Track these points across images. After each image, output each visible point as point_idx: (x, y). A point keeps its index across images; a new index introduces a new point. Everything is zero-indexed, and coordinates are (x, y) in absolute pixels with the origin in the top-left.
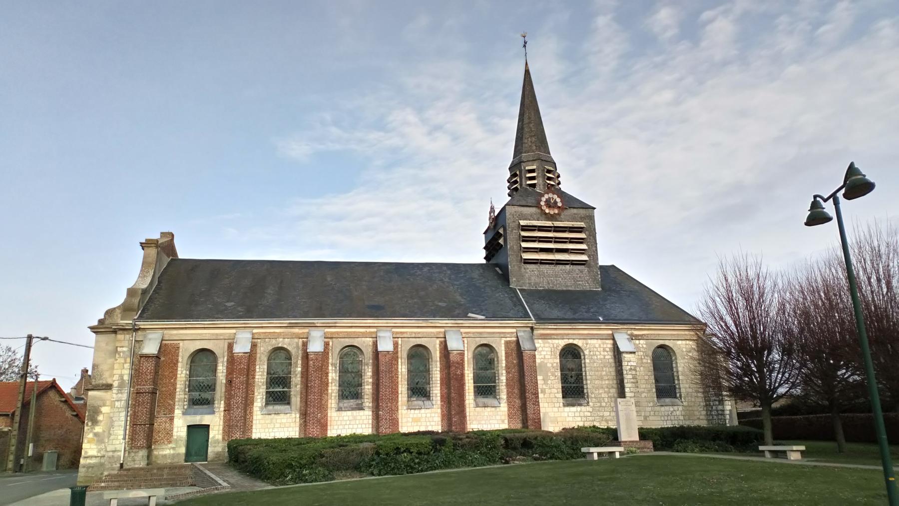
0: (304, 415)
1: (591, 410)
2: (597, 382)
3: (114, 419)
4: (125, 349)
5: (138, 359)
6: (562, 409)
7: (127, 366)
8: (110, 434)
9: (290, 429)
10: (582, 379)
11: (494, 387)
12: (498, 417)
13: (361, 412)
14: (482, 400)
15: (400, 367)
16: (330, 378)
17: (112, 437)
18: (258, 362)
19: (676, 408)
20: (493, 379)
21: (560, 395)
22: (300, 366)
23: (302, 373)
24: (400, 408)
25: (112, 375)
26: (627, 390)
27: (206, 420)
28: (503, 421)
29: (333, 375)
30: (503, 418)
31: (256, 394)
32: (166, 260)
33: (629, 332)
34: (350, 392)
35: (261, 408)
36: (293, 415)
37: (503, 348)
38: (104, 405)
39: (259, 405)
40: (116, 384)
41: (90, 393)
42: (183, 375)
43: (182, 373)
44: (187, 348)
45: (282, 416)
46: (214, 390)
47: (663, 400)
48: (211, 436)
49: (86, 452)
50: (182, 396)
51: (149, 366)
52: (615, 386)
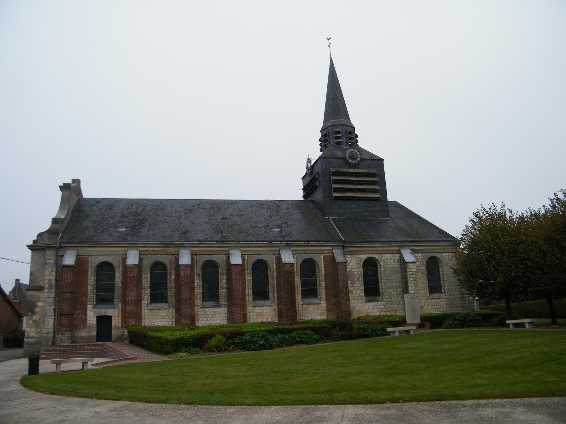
0: (178, 311)
1: (384, 304)
2: (389, 284)
3: (46, 311)
4: (52, 261)
5: (61, 269)
6: (364, 304)
7: (53, 273)
8: (44, 322)
9: (169, 320)
10: (378, 282)
11: (316, 290)
12: (319, 311)
13: (219, 309)
14: (307, 300)
15: (246, 276)
16: (196, 284)
17: (46, 323)
18: (143, 272)
19: (442, 300)
20: (315, 284)
21: (363, 294)
22: (173, 275)
23: (175, 279)
24: (247, 305)
25: (44, 280)
26: (410, 289)
27: (110, 312)
28: (323, 314)
29: (198, 282)
30: (323, 311)
31: (143, 295)
32: (76, 198)
33: (411, 248)
34: (211, 296)
35: (147, 305)
36: (171, 310)
37: (323, 262)
38: (39, 301)
39: (146, 302)
40: (46, 286)
41: (30, 292)
42: (92, 280)
43: (91, 280)
44: (94, 262)
45: (162, 311)
46: (114, 291)
47: (433, 295)
48: (113, 324)
49: (28, 334)
50: (92, 295)
51: (68, 274)
52: (401, 286)
